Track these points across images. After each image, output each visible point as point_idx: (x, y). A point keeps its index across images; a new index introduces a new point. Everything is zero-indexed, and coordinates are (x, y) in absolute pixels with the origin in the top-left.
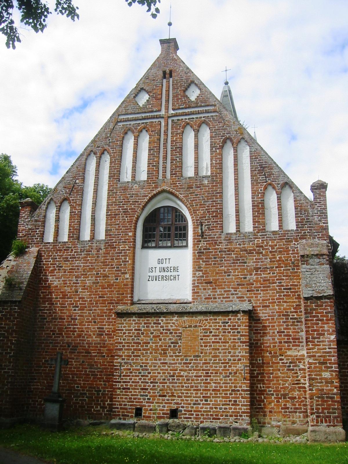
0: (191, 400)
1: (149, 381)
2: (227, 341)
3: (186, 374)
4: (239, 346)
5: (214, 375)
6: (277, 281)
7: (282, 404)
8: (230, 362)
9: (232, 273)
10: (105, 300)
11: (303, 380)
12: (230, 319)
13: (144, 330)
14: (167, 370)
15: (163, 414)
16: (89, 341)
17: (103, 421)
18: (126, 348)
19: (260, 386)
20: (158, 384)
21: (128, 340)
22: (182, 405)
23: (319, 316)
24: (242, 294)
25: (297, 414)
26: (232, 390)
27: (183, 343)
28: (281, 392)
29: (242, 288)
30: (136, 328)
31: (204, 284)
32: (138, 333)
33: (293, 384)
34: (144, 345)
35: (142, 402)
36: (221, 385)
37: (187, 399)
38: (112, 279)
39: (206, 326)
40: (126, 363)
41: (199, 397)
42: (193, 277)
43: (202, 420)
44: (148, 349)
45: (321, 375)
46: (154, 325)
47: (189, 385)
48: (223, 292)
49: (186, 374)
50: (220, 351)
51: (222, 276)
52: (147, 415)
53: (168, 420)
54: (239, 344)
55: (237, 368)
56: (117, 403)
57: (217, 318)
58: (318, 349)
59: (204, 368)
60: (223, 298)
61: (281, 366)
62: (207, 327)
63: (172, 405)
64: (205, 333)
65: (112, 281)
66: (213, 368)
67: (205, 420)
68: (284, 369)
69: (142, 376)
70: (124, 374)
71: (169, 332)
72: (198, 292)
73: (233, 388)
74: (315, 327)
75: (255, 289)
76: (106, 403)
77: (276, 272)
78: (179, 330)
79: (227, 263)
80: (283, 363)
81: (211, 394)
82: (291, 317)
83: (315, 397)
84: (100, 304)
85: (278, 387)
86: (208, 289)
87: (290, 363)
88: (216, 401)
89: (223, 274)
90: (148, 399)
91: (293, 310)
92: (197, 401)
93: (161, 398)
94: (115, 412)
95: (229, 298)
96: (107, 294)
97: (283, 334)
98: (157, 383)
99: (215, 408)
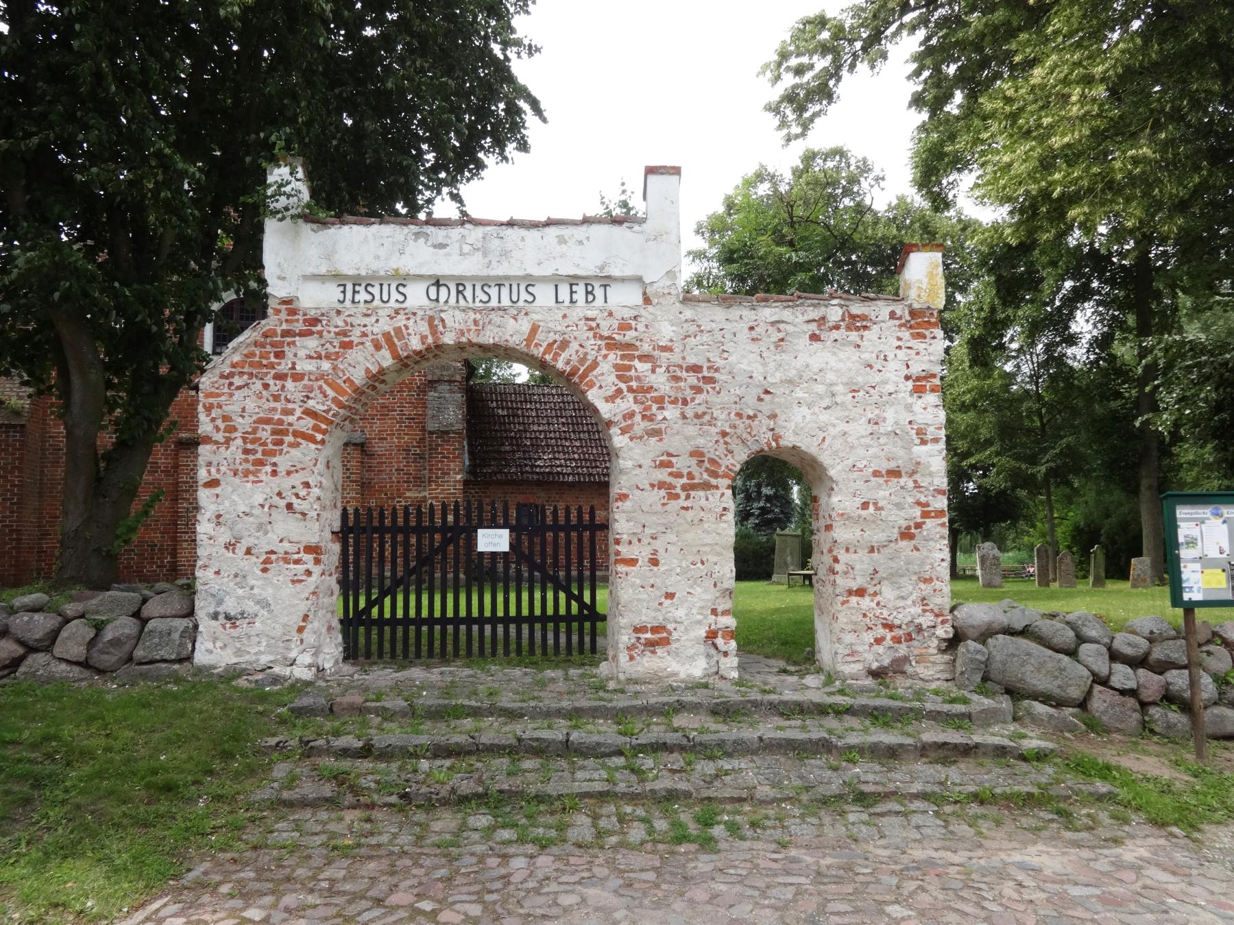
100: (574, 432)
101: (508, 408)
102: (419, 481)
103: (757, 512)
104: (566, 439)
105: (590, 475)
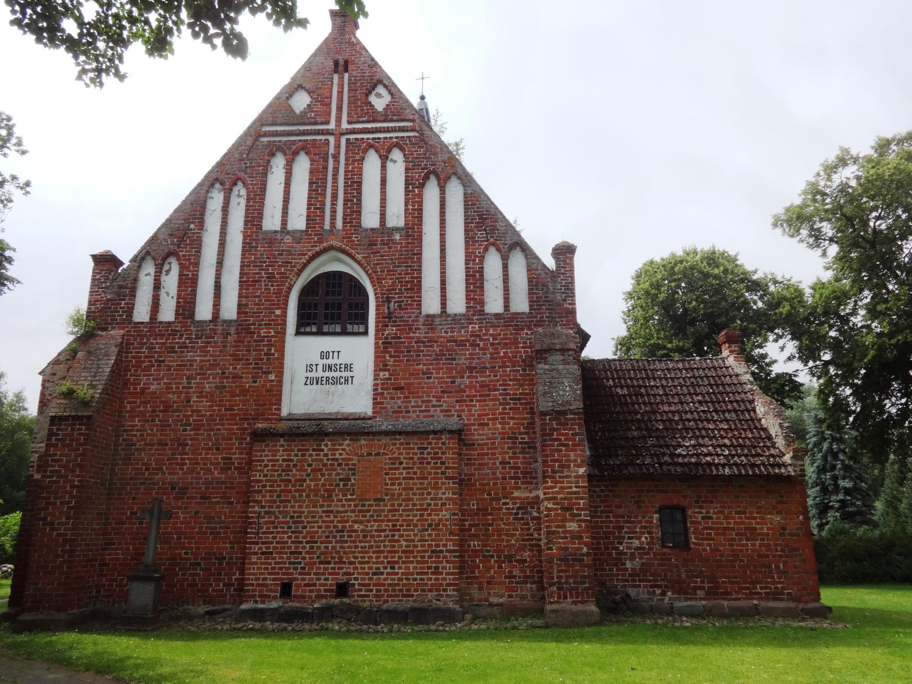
3: (362, 527)
4: (443, 484)
10: (236, 415)
12: (430, 443)
13: (298, 461)
14: (332, 522)
15: (326, 591)
17: (227, 606)
18: (268, 488)
20: (319, 544)
22: (356, 576)
24: (449, 406)
25: (529, 585)
26: (433, 551)
29: (448, 397)
32: (288, 466)
33: (522, 540)
35: (292, 574)
39: (394, 453)
40: (266, 513)
41: (382, 563)
42: (375, 379)
45: (564, 526)
49: (362, 527)
52: (299, 593)
53: (333, 600)
58: (561, 488)
59: (390, 517)
60: (420, 411)
62: (396, 455)
64: (392, 464)
69: (292, 532)
70: (264, 530)
71: (336, 464)
72: (382, 403)
78: (352, 460)
81: (400, 557)
84: (227, 420)
86: (399, 398)
87: (518, 508)
92: (379, 568)
93: (322, 566)
94: (248, 591)
95: (429, 411)
98: (317, 542)
99: (408, 579)
100: (716, 411)
101: (628, 387)
102: (529, 477)
103: (837, 505)
104: (708, 421)
105: (753, 466)
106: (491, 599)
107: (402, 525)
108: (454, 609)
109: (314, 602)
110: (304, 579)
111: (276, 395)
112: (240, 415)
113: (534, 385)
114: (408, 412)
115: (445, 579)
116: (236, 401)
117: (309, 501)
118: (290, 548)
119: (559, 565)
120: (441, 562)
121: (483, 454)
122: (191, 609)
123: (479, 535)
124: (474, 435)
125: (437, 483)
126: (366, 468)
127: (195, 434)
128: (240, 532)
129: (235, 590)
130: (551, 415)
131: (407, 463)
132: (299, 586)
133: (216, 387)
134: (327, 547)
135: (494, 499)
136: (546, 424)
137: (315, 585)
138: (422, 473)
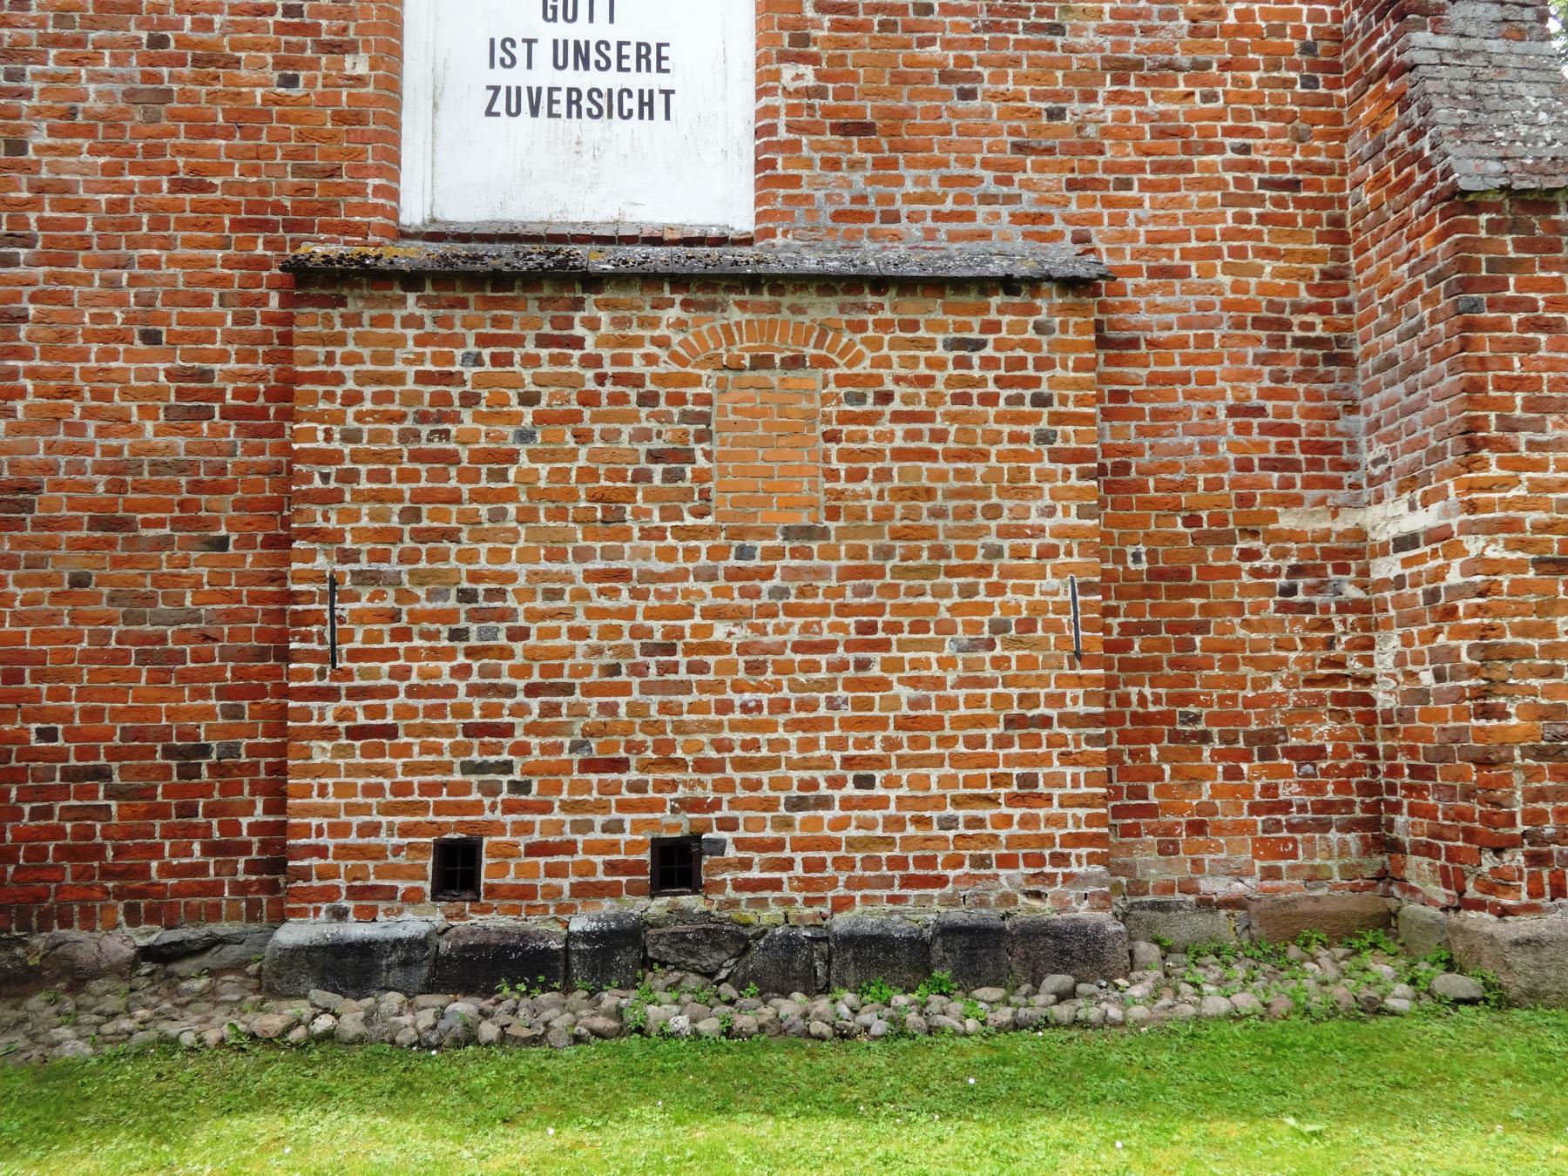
0: (776, 784)
1: (521, 684)
2: (980, 445)
3: (742, 634)
4: (1044, 476)
5: (905, 635)
6: (1228, 141)
7: (1252, 787)
8: (996, 563)
9: (986, 85)
10: (215, 207)
11: (1361, 659)
12: (994, 327)
13: (480, 381)
14: (629, 613)
15: (611, 868)
16: (119, 451)
17: (223, 928)
18: (364, 485)
19: (1140, 694)
20: (578, 697)
21: (376, 437)
22: (725, 812)
23: (1541, 304)
24: (1040, 201)
25: (1333, 835)
26: (1011, 722)
27: (725, 456)
28: (1248, 723)
29: (1040, 168)
30: (428, 367)
31: (828, 137)
32: (442, 399)
33: (1309, 682)
34: (484, 469)
35: (477, 807)
36: (950, 692)
37: (753, 775)
38: (257, 81)
39: (858, 358)
40: (361, 578)
41: (825, 763)
42: (760, 93)
43: (841, 891)
44: (511, 495)
45: (1548, 630)
46: (544, 353)
47: (764, 698)
48: (935, 187)
49: (742, 634)
50: (939, 501)
51: (932, 95)
52: (510, 879)
53: (643, 902)
54: (1046, 464)
55: (1037, 597)
56: (315, 821)
57: (922, 319)
58: (1535, 486)
59: (849, 599)
60: (937, 216)
61: (1245, 590)
62: (864, 368)
63: (665, 816)
64: (850, 398)
65: (259, 92)
66: (903, 600)
67: (858, 894)
68: (1265, 606)
69: (471, 653)
70: (357, 644)
71: (633, 394)
72: (795, 181)
73: (1016, 711)
74: (1517, 364)
75: (1112, 177)
76: (245, 821)
77: (1220, 90)
78: (697, 381)
79: (956, 27)
80: (1257, 573)
81: (891, 744)
82: (1298, 333)
83: (1517, 753)
84: (182, 224)
85: (1234, 698)
86: (854, 165)
87: (1295, 571)
88: (922, 782)
89: (936, 85)
90: (517, 787)
91: (1304, 296)
92: (812, 785)
93: (594, 778)
94: (305, 874)
95: (971, 217)
96: (225, 169)
97: (1255, 422)
98: (568, 690)
99: (920, 822)
106: (1207, 885)
107: (894, 628)
108: (1099, 927)
109: (570, 909)
110: (526, 828)
111: (380, 136)
112: (235, 207)
113: (1344, 136)
114: (893, 217)
115: (1059, 821)
116: (215, 152)
117: (532, 535)
118: (462, 711)
119: (1531, 774)
120: (1045, 760)
121: (1171, 379)
122: (85, 943)
123: (1156, 665)
124: (1133, 307)
125: (1022, 474)
126: (753, 413)
127: (49, 278)
128: (261, 655)
129: (251, 867)
130: (1498, 208)
131: (906, 399)
132: (508, 851)
133: (129, 95)
134: (611, 709)
135: (1210, 538)
136: (1476, 246)
137: (569, 848)
138: (963, 435)
